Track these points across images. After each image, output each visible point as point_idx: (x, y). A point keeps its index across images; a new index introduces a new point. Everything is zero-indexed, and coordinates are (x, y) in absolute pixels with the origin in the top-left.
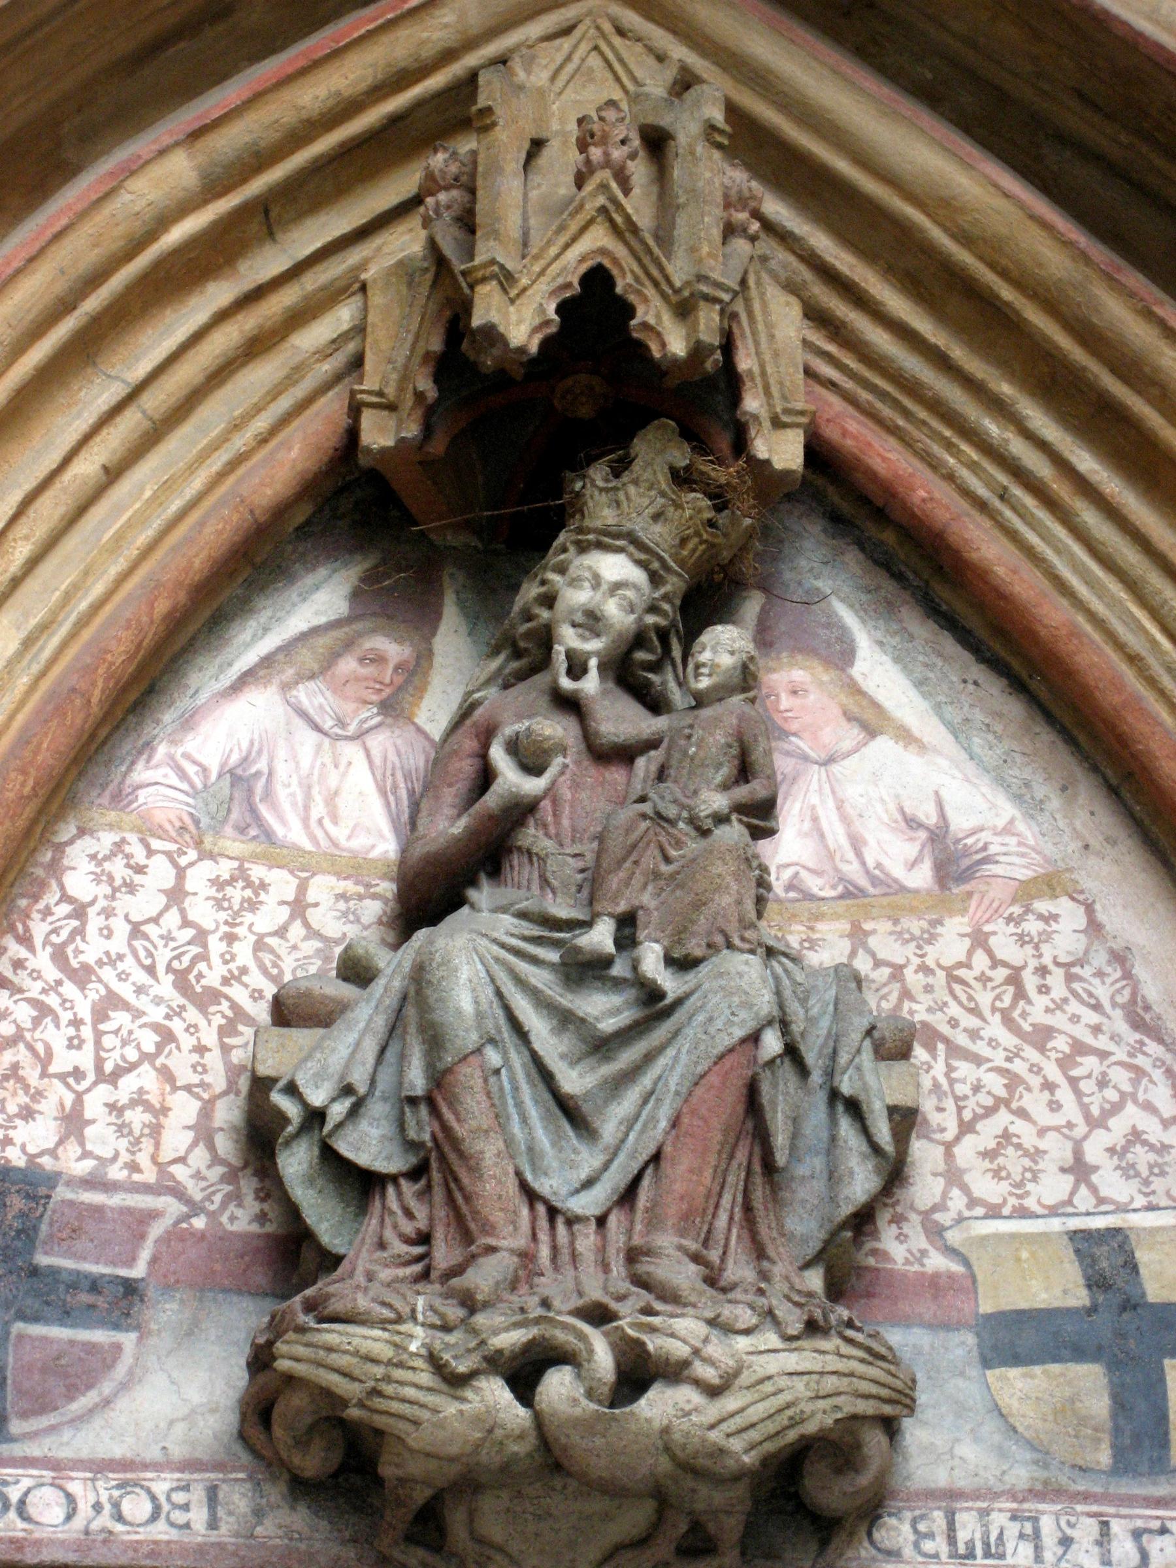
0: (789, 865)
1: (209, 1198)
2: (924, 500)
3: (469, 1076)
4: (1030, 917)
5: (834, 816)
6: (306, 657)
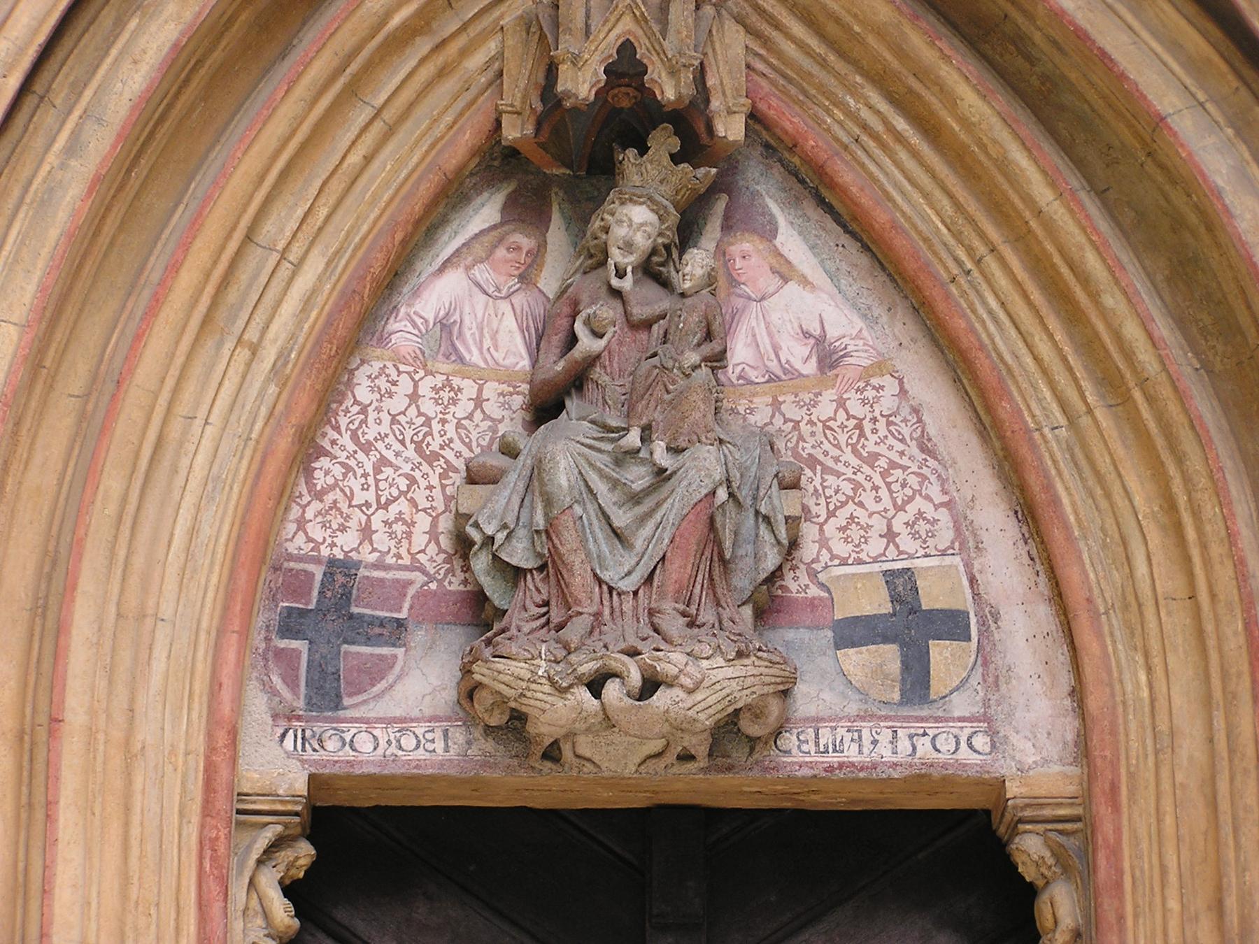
0: (739, 364)
1: (437, 572)
2: (813, 147)
3: (567, 520)
4: (869, 388)
5: (764, 333)
6: (478, 249)
